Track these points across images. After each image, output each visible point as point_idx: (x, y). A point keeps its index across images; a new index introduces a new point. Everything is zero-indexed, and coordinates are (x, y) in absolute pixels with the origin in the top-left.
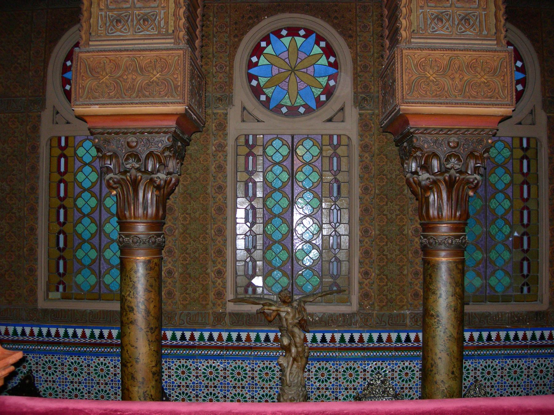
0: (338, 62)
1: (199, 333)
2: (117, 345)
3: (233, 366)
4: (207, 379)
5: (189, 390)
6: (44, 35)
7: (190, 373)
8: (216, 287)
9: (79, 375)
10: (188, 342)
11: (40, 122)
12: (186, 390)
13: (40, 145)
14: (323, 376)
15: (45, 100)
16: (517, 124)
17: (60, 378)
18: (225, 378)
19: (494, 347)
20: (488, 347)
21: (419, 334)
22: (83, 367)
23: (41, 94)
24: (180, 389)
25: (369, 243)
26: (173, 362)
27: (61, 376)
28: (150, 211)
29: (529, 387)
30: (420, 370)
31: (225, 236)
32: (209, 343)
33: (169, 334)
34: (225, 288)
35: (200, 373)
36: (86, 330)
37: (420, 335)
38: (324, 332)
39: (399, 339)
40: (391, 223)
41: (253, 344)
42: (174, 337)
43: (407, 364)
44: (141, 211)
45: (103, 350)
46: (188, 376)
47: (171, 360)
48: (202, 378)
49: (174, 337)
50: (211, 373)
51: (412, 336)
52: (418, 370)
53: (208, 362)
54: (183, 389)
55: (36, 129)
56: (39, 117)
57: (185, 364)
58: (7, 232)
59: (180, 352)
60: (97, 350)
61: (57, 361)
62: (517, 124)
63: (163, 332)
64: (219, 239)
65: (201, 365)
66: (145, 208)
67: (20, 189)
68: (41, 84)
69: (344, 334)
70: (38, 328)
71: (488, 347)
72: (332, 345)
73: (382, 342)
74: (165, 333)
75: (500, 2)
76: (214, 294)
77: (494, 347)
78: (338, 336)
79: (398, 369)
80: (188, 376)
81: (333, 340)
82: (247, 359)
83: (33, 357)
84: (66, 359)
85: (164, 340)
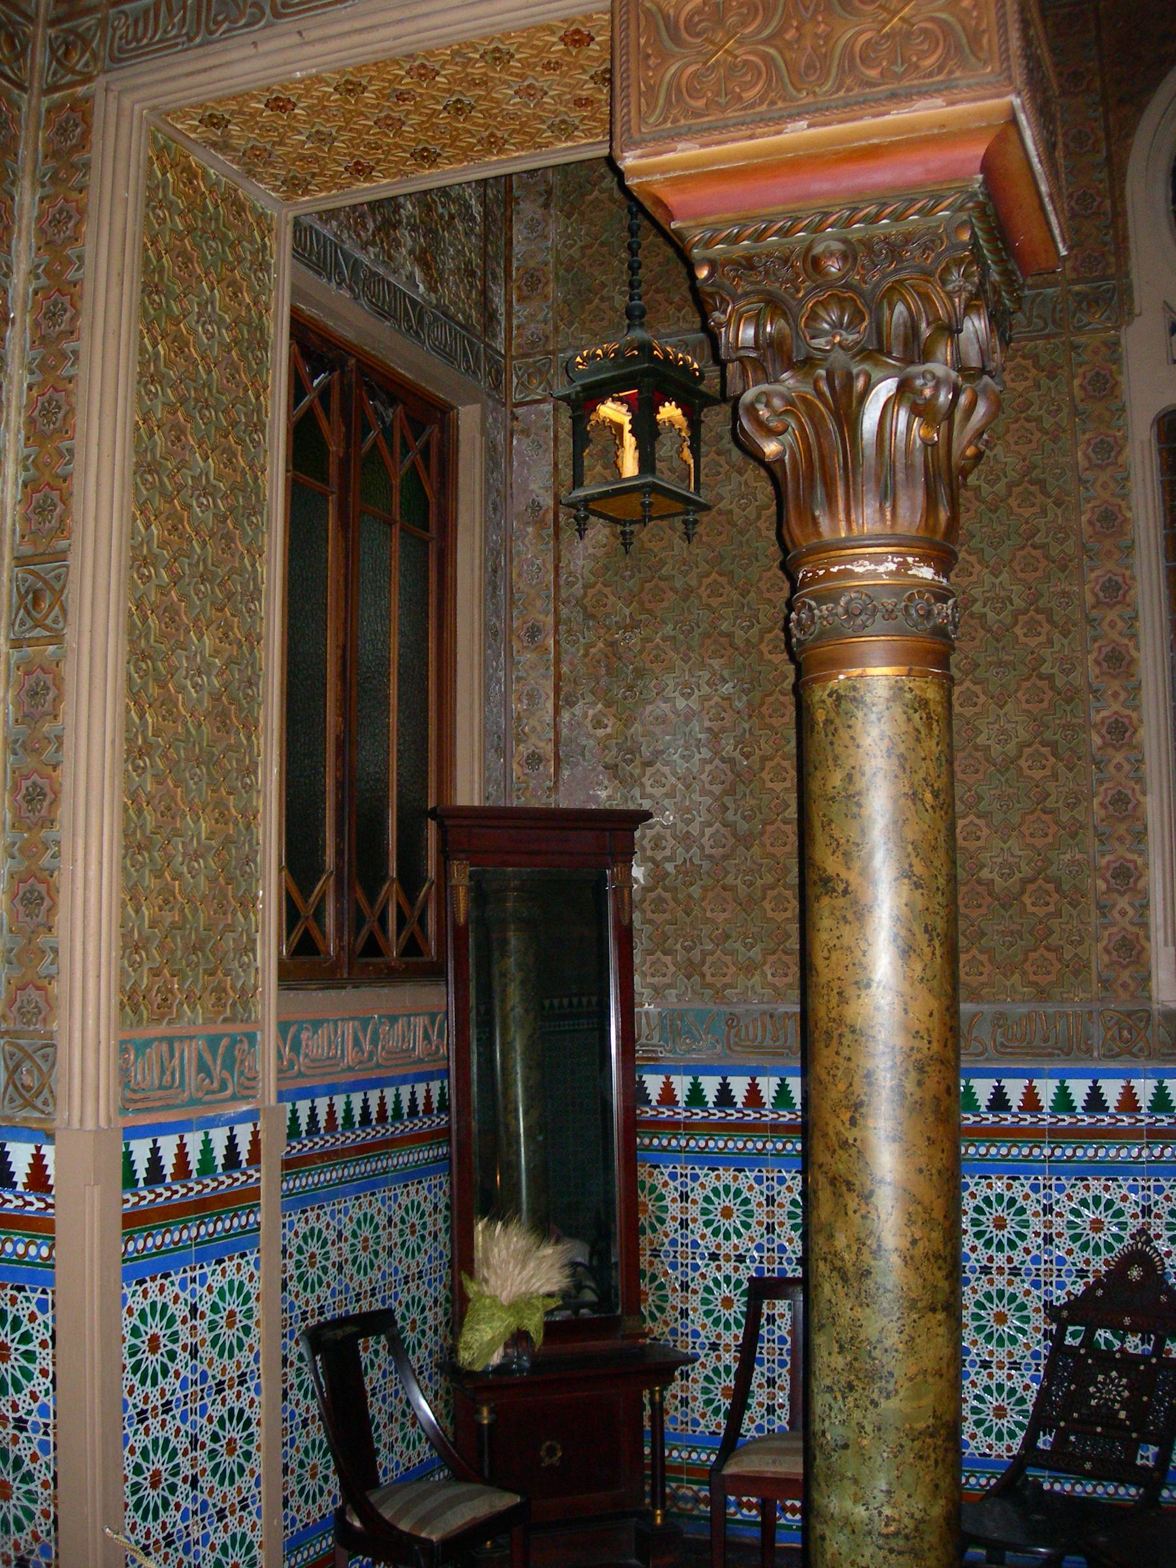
0: (313, 312)
3: (1077, 1197)
4: (1084, 1247)
5: (1020, 1286)
6: (1097, 84)
7: (1025, 1224)
8: (1112, 925)
10: (1112, 1116)
11: (1117, 361)
12: (1010, 1283)
13: (1125, 438)
15: (1129, 289)
18: (1048, 1239)
19: (740, 1128)
20: (725, 1127)
21: (789, 1080)
22: (752, 1206)
23: (1111, 271)
24: (991, 1282)
25: (1127, 767)
26: (1060, 1189)
27: (764, 1241)
31: (1139, 748)
32: (719, 1115)
33: (983, 1089)
34: (1145, 925)
35: (1059, 1224)
37: (795, 1085)
38: (1062, 1075)
40: (1068, 702)
42: (999, 1102)
43: (999, 1186)
45: (779, 1146)
46: (1018, 1234)
47: (1152, 1183)
48: (1065, 1243)
49: (999, 1102)
50: (1097, 1225)
51: (768, 1087)
53: (1087, 1188)
54: (1001, 1281)
55: (1105, 386)
56: (1114, 345)
57: (1007, 1195)
60: (721, 1144)
61: (751, 1188)
63: (963, 1082)
64: (1119, 757)
65: (1063, 1197)
67: (1064, 594)
68: (1108, 238)
69: (1068, 1083)
70: (689, 1079)
71: (725, 1127)
72: (1127, 1120)
74: (968, 1088)
75: (1012, 8)
76: (1106, 950)
77: (740, 1128)
78: (1047, 1090)
80: (1018, 1234)
81: (1031, 1102)
82: (1028, 1172)
83: (759, 1180)
84: (695, 1178)
85: (967, 1110)
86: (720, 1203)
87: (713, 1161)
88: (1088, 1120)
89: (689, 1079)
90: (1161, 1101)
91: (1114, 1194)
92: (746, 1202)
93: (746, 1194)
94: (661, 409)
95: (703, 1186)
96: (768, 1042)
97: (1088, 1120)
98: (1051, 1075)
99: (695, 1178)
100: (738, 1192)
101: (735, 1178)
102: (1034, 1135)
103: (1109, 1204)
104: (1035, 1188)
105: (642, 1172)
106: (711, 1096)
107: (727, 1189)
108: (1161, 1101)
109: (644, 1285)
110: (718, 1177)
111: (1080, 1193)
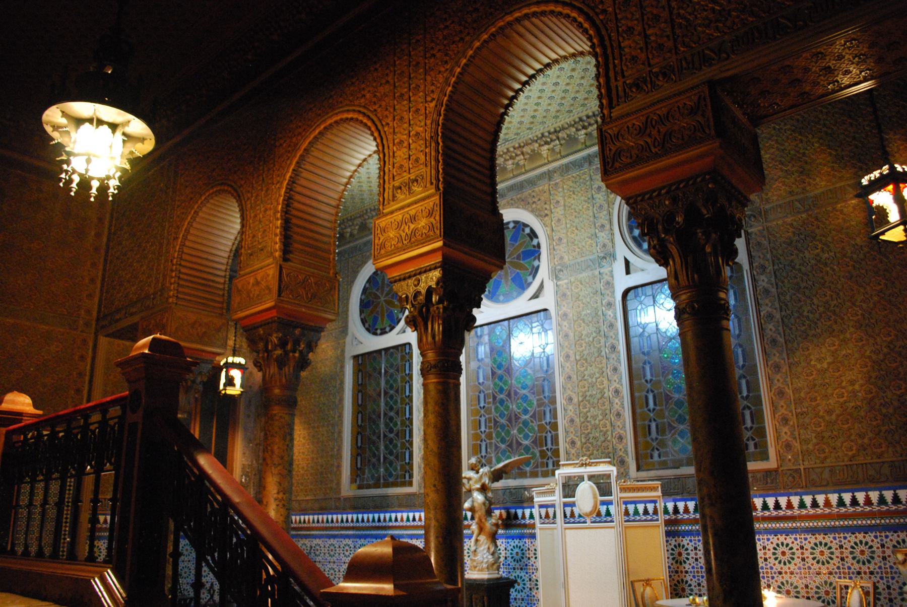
1: (836, 496)
2: (695, 521)
9: (790, 562)
14: (822, 555)
16: (530, 299)
17: (799, 568)
19: (809, 517)
28: (437, 338)
29: (770, 575)
30: (895, 532)
36: (830, 496)
37: (109, 518)
38: (788, 495)
39: (841, 503)
41: (797, 512)
44: (430, 339)
52: (853, 536)
58: (838, 416)
59: (773, 525)
62: (530, 299)
66: (434, 337)
70: (837, 495)
72: (868, 509)
73: (859, 505)
79: (771, 547)
86: (781, 549)
87: (776, 532)
88: (894, 508)
89: (786, 498)
90: (896, 500)
91: (789, 541)
92: (871, 547)
93: (870, 543)
94: (475, 311)
95: (849, 541)
96: (849, 479)
97: (894, 508)
98: (796, 494)
99: (768, 540)
100: (866, 543)
101: (864, 537)
102: (792, 518)
103: (826, 544)
104: (835, 538)
105: (96, 543)
106: (681, 509)
107: (861, 542)
108: (896, 500)
109: (96, 549)
110: (856, 537)
111: (775, 541)
